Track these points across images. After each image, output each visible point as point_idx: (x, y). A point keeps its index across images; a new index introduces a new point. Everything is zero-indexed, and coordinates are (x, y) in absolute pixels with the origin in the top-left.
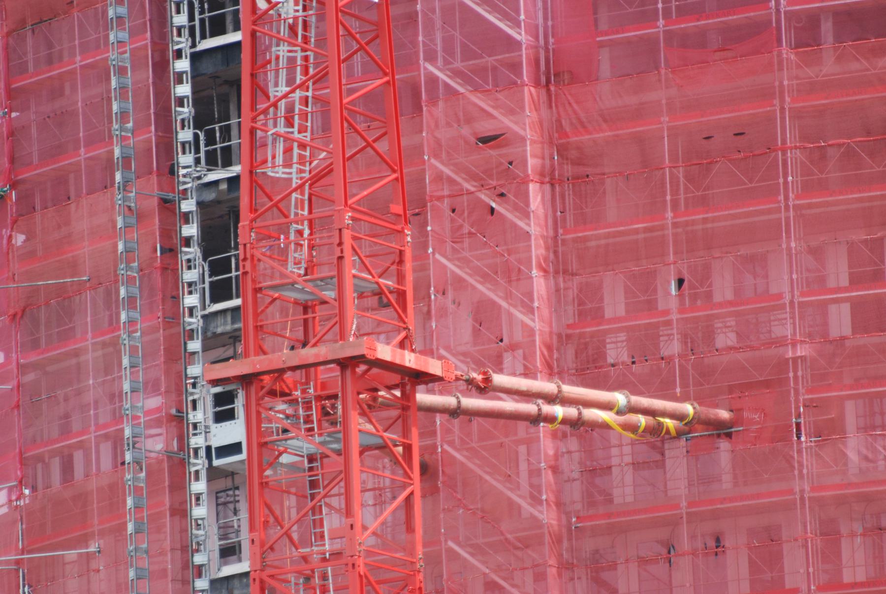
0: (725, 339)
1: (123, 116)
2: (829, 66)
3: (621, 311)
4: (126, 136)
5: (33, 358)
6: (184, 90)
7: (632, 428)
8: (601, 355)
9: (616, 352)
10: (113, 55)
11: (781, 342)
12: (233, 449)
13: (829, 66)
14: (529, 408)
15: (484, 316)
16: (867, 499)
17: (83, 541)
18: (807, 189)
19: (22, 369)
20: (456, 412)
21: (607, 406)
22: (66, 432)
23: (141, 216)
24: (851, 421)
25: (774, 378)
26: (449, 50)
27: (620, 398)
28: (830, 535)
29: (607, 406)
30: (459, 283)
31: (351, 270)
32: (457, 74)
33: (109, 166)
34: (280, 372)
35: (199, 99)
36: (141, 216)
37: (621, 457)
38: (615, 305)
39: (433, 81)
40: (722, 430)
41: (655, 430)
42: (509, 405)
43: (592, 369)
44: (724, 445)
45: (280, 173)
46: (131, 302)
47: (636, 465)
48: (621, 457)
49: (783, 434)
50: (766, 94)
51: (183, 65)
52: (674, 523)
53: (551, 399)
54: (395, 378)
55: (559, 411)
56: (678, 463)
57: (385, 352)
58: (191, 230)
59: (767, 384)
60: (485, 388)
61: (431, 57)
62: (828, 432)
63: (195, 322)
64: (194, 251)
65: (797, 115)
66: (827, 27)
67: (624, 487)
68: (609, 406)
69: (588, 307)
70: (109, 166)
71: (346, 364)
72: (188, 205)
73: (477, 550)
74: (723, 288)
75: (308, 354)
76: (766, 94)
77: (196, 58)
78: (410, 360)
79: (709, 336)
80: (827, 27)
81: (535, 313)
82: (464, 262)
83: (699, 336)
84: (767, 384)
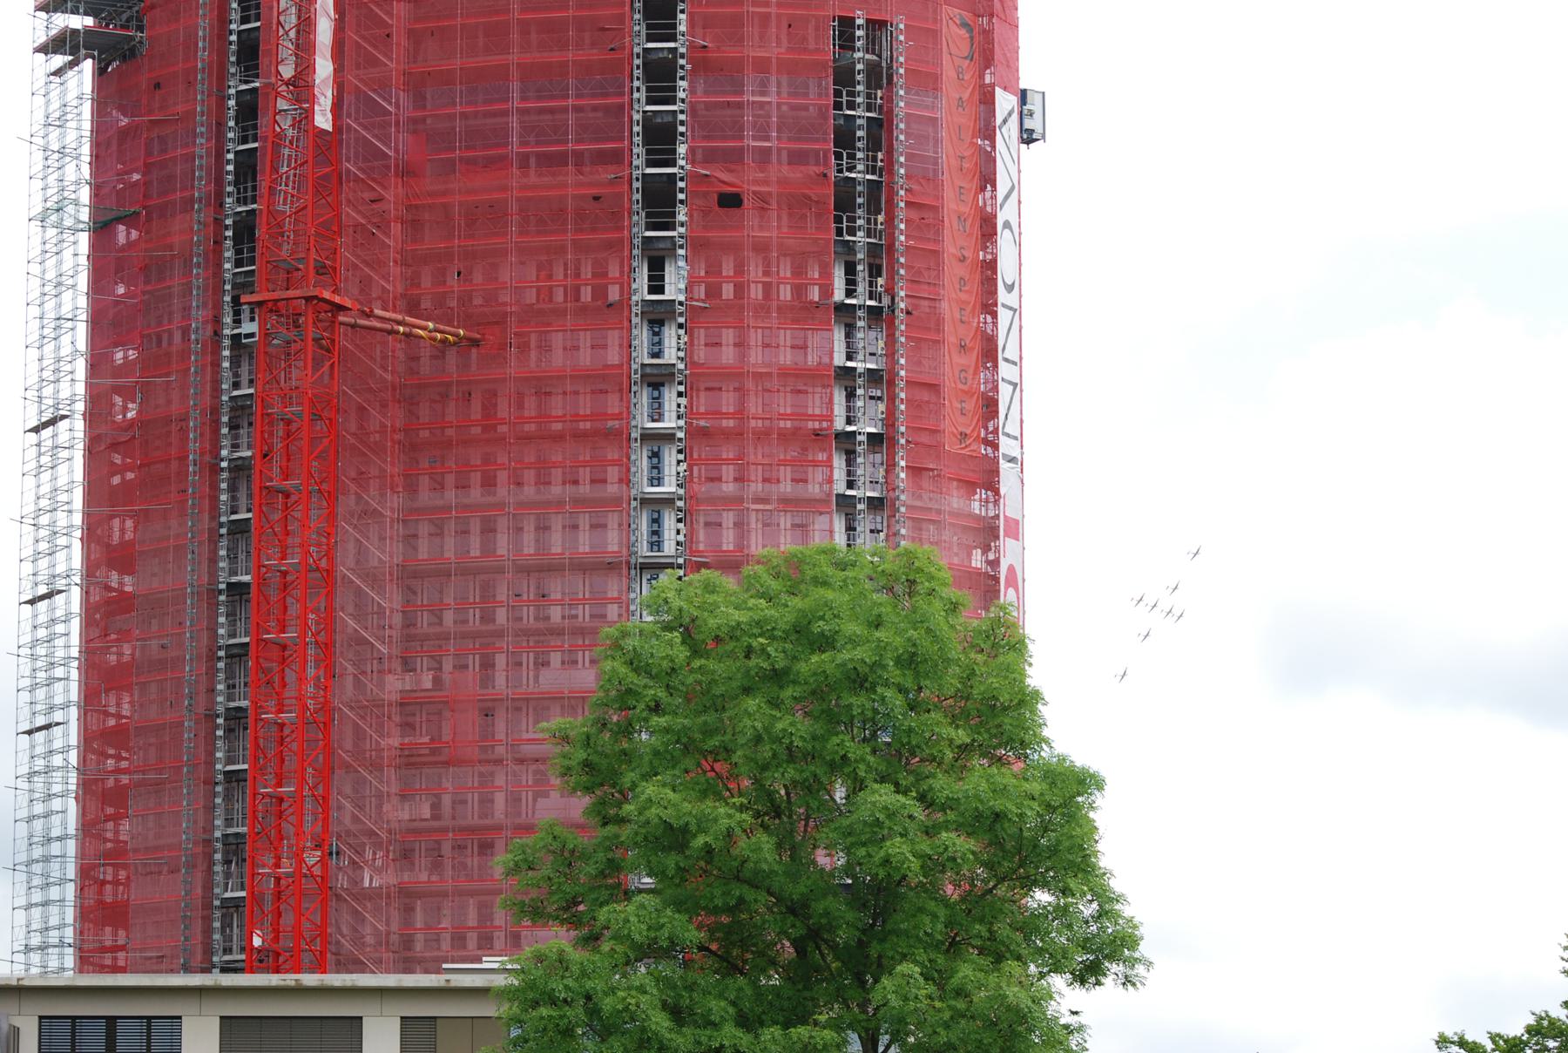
0: (477, 301)
1: (201, 179)
2: (533, 178)
3: (731, 273)
4: (201, 186)
5: (148, 288)
6: (230, 168)
7: (434, 339)
8: (419, 304)
9: (426, 304)
10: (198, 150)
11: (505, 304)
12: (252, 335)
13: (533, 178)
14: (388, 327)
15: (365, 284)
16: (538, 379)
17: (168, 375)
18: (521, 234)
19: (144, 293)
20: (353, 326)
21: (424, 328)
22: (160, 324)
23: (206, 225)
24: (533, 344)
25: (501, 321)
26: (356, 157)
27: (431, 325)
28: (520, 397)
29: (424, 328)
30: (355, 267)
31: (313, 255)
32: (359, 169)
33: (192, 200)
34: (276, 301)
35: (236, 173)
36: (206, 225)
37: (425, 353)
38: (426, 282)
39: (348, 170)
40: (475, 343)
41: (444, 341)
42: (378, 325)
43: (413, 308)
44: (474, 350)
45: (281, 208)
46: (199, 265)
47: (433, 357)
48: (425, 353)
49: (503, 347)
50: (505, 189)
51: (230, 156)
52: (449, 385)
53: (399, 323)
54: (328, 307)
55: (401, 329)
56: (452, 357)
57: (326, 295)
58: (229, 233)
59: (497, 323)
60: (369, 315)
61: (348, 161)
62: (524, 348)
63: (228, 276)
64: (229, 243)
65: (518, 199)
66: (532, 161)
67: (426, 367)
68: (426, 328)
69: (414, 281)
70: (192, 200)
71: (308, 299)
72: (229, 222)
73: (356, 391)
74: (478, 278)
75: (291, 293)
76: (505, 189)
77: (237, 153)
78: (337, 299)
79: (471, 300)
80: (532, 161)
81: (393, 281)
82: (358, 257)
83: (465, 299)
84: (497, 323)
